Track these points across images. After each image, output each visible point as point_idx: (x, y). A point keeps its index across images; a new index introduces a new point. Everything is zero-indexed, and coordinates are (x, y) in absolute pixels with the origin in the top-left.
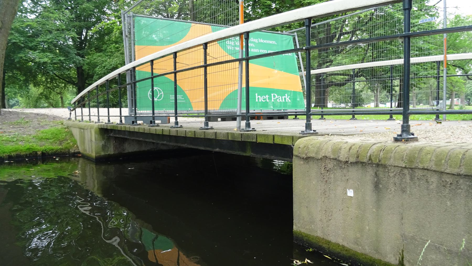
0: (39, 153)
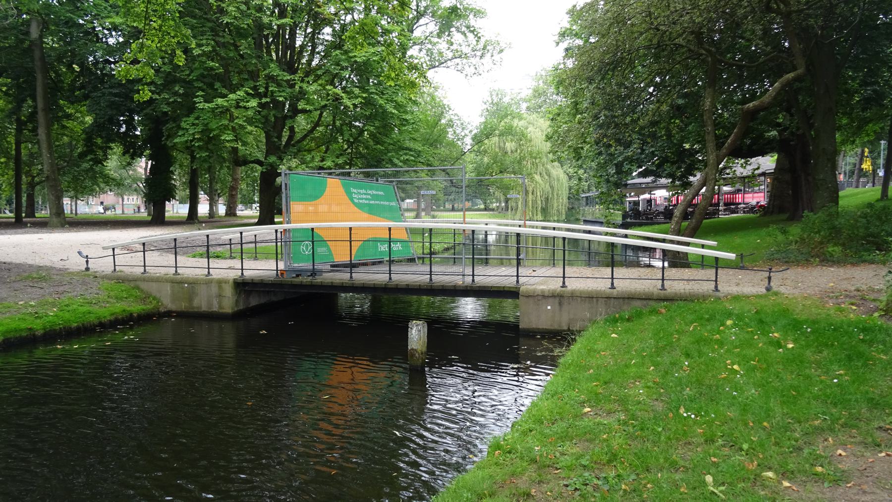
0: (135, 315)
